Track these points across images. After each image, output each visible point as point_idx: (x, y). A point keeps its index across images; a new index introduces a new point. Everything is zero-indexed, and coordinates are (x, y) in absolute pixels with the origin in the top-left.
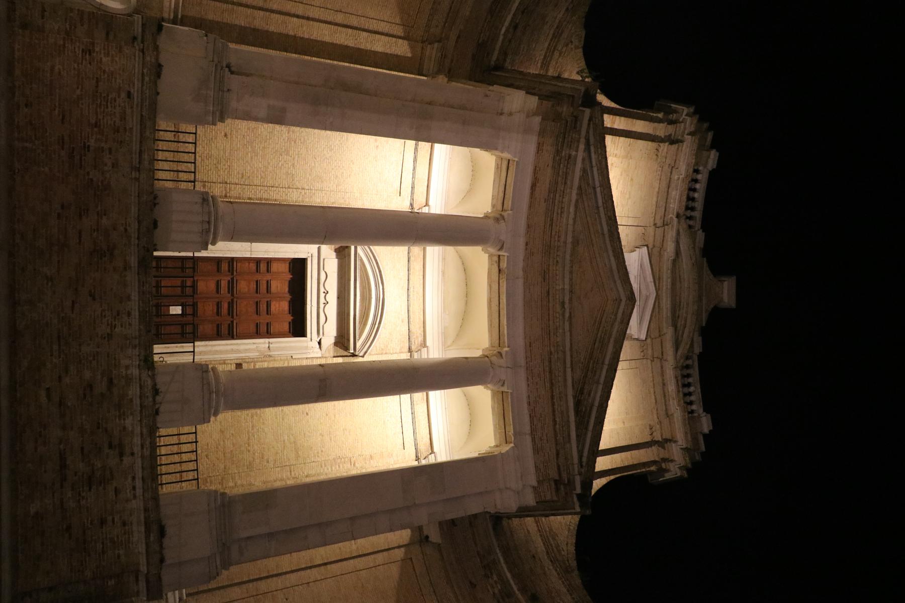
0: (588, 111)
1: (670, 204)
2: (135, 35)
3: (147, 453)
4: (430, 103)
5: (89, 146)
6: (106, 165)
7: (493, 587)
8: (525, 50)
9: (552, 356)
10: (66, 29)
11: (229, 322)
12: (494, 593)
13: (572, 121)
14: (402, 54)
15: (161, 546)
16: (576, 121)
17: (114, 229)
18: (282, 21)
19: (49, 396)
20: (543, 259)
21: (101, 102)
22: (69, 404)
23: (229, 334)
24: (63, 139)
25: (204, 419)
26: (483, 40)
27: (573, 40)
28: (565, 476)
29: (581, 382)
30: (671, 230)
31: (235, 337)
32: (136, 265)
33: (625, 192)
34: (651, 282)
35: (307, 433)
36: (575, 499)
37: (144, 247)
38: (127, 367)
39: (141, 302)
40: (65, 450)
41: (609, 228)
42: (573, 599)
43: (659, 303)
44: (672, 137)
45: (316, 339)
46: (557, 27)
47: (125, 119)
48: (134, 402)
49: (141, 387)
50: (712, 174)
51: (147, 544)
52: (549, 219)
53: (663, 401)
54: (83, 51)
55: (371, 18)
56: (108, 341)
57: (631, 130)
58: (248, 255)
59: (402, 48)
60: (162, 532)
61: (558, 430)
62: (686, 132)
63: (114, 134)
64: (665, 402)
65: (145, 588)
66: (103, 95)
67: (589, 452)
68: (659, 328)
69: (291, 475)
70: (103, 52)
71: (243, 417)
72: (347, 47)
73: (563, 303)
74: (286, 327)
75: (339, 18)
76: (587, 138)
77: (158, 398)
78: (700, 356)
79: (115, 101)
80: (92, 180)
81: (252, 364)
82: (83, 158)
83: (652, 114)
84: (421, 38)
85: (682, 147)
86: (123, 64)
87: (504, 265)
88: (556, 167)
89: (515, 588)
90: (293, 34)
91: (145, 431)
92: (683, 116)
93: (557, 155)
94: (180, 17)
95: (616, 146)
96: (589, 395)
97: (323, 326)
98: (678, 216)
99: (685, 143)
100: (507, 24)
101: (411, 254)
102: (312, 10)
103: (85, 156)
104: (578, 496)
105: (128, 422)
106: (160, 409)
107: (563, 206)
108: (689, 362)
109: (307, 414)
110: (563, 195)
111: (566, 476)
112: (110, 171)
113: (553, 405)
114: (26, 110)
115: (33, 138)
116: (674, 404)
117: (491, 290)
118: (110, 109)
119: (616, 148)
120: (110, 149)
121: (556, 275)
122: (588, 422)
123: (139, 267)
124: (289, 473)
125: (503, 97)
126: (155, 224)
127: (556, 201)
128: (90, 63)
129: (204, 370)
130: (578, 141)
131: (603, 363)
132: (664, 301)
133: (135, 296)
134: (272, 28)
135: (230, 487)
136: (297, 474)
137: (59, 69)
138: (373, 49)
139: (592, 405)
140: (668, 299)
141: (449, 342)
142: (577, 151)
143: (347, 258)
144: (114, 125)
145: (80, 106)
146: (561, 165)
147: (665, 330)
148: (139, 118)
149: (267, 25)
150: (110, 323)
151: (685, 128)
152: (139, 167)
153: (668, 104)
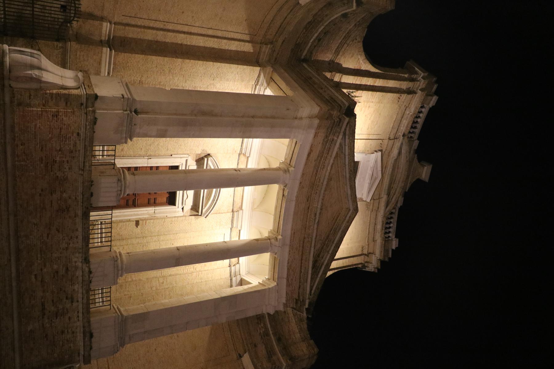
0: (347, 119)
1: (401, 127)
2: (82, 102)
3: (85, 301)
4: (253, 117)
5: (56, 161)
6: (65, 168)
7: (260, 329)
8: (326, 44)
9: (305, 240)
10: (43, 103)
11: (134, 199)
12: (260, 332)
13: (337, 122)
14: (248, 51)
15: (91, 342)
16: (340, 122)
17: (70, 198)
18: (174, 36)
19: (36, 278)
20: (309, 190)
21: (63, 139)
22: (46, 281)
23: (133, 204)
24: (42, 159)
25: (114, 283)
26: (299, 42)
27: (357, 38)
28: (301, 298)
29: (319, 250)
30: (398, 142)
31: (136, 206)
32: (81, 215)
33: (375, 121)
34: (380, 171)
36: (304, 310)
37: (85, 207)
38: (76, 262)
39: (83, 233)
40: (44, 301)
41: (350, 175)
42: (301, 336)
43: (382, 180)
44: (411, 89)
45: (181, 207)
46: (348, 33)
47: (76, 146)
48: (79, 278)
49: (82, 272)
50: (431, 110)
51: (84, 342)
52: (316, 170)
53: (373, 233)
54: (52, 115)
55: (230, 32)
56: (66, 250)
57: (385, 86)
58: (146, 165)
59: (247, 48)
60: (91, 336)
61: (302, 276)
62: (420, 88)
63: (70, 153)
64: (374, 233)
65: (82, 359)
66: (64, 136)
67: (316, 288)
68: (380, 194)
69: (161, 275)
70: (64, 115)
71: (138, 247)
72: (213, 48)
73: (316, 214)
74: (165, 200)
75: (210, 32)
76: (344, 133)
77: (91, 275)
78: (400, 209)
79: (70, 138)
80: (58, 176)
81: (145, 221)
82: (53, 166)
83: (401, 75)
84: (260, 41)
85: (415, 96)
86: (75, 120)
87: (286, 194)
88: (324, 144)
89: (271, 332)
90: (180, 43)
91: (84, 292)
92: (420, 78)
93: (326, 138)
94: (112, 38)
95: (374, 97)
96: (322, 258)
97: (185, 201)
98: (404, 135)
99: (417, 94)
100: (314, 38)
101: (239, 161)
102: (193, 29)
103: (54, 165)
104: (307, 309)
105: (76, 287)
106: (92, 280)
107: (325, 165)
108: (394, 211)
110: (326, 159)
111: (302, 298)
112: (67, 171)
113: (301, 263)
114: (21, 147)
115: (26, 160)
116: (378, 235)
117: (277, 202)
118: (67, 142)
119: (373, 98)
120: (68, 161)
121: (315, 199)
122: (319, 272)
123: (82, 216)
124: (161, 274)
125: (298, 109)
126: (92, 195)
127: (321, 162)
128: (57, 121)
129: (115, 260)
130: (339, 133)
131: (333, 242)
132: (386, 180)
133: (80, 230)
134: (168, 40)
135: (130, 281)
136: (165, 275)
137: (39, 125)
138: (229, 49)
139: (323, 264)
140: (388, 180)
141: (255, 207)
142: (338, 138)
143: (202, 165)
144: (70, 149)
145: (51, 142)
146: (327, 143)
147: (382, 196)
148: (84, 146)
149: (165, 38)
150: (67, 242)
151: (419, 86)
152: (83, 169)
153: (414, 66)
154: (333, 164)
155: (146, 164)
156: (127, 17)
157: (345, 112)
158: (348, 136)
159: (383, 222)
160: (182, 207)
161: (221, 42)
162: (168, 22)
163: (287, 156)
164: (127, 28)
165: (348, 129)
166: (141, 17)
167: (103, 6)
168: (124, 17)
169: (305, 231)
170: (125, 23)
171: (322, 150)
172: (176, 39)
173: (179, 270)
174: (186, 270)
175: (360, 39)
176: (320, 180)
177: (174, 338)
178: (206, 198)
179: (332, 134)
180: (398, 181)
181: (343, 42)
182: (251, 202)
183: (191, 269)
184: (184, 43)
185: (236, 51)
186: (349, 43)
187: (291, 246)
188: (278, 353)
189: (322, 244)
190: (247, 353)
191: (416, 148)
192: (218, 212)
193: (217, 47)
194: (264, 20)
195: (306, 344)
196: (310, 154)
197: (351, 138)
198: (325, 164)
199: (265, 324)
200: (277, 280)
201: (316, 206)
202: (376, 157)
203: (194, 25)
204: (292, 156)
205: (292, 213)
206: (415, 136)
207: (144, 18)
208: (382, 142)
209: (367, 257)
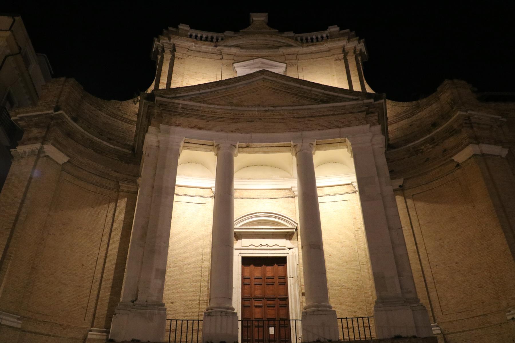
0: (157, 98)
1: (209, 51)
4: (153, 187)
9: (296, 117)
14: (126, 203)
27: (117, 107)
31: (287, 297)
34: (253, 61)
35: (341, 255)
43: (265, 56)
44: (171, 50)
45: (288, 251)
50: (192, 27)
53: (321, 53)
58: (240, 290)
59: (122, 204)
61: (338, 113)
62: (169, 42)
67: (350, 95)
69: (365, 264)
71: (333, 292)
72: (122, 234)
73: (266, 111)
74: (281, 268)
75: (105, 239)
78: (296, 33)
84: (116, 192)
87: (244, 144)
88: (188, 115)
89: (428, 136)
90: (115, 265)
92: (160, 44)
94: (105, 330)
96: (317, 95)
97: (280, 247)
98: (216, 46)
99: (175, 43)
100: (108, 144)
101: (239, 197)
107: (211, 111)
108: (299, 39)
109: (330, 255)
110: (204, 111)
111: (364, 108)
113: (323, 116)
117: (258, 152)
121: (250, 115)
124: (365, 265)
130: (174, 103)
131: (300, 88)
132: (265, 53)
134: (112, 277)
141: (289, 175)
142: (179, 104)
143: (241, 234)
147: (281, 53)
149: (109, 280)
151: (167, 43)
153: (153, 52)
154: (208, 104)
155: (239, 290)
156: (86, 316)
157: (151, 101)
158: (177, 94)
159: (308, 46)
160: (287, 249)
161: (116, 228)
162: (93, 278)
163: (208, 150)
164: (97, 316)
165: (168, 96)
166: (87, 303)
167: (72, 338)
168: (86, 319)
169: (286, 118)
170: (92, 318)
171: (195, 116)
172: (111, 269)
173: (360, 246)
174: (361, 238)
175: (118, 104)
176: (228, 114)
177: (442, 243)
178: (278, 226)
179: (177, 109)
180: (266, 41)
181: (120, 118)
182: (283, 180)
183: (359, 234)
184: (115, 262)
185: (125, 213)
186: (122, 113)
187: (303, 130)
188: (448, 123)
189: (304, 99)
190: (452, 158)
191: (233, 32)
192: (295, 212)
193: (121, 231)
194: (93, 191)
195: (441, 96)
196: (199, 127)
197: (179, 91)
198: (209, 111)
199: (421, 145)
200: (343, 138)
201: (257, 112)
202: (238, 67)
203: (98, 254)
204: (201, 144)
205: (266, 135)
206: (220, 36)
207: (88, 300)
208: (224, 65)
209: (349, 53)
